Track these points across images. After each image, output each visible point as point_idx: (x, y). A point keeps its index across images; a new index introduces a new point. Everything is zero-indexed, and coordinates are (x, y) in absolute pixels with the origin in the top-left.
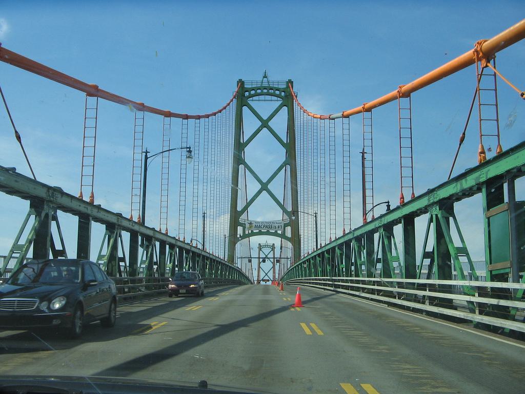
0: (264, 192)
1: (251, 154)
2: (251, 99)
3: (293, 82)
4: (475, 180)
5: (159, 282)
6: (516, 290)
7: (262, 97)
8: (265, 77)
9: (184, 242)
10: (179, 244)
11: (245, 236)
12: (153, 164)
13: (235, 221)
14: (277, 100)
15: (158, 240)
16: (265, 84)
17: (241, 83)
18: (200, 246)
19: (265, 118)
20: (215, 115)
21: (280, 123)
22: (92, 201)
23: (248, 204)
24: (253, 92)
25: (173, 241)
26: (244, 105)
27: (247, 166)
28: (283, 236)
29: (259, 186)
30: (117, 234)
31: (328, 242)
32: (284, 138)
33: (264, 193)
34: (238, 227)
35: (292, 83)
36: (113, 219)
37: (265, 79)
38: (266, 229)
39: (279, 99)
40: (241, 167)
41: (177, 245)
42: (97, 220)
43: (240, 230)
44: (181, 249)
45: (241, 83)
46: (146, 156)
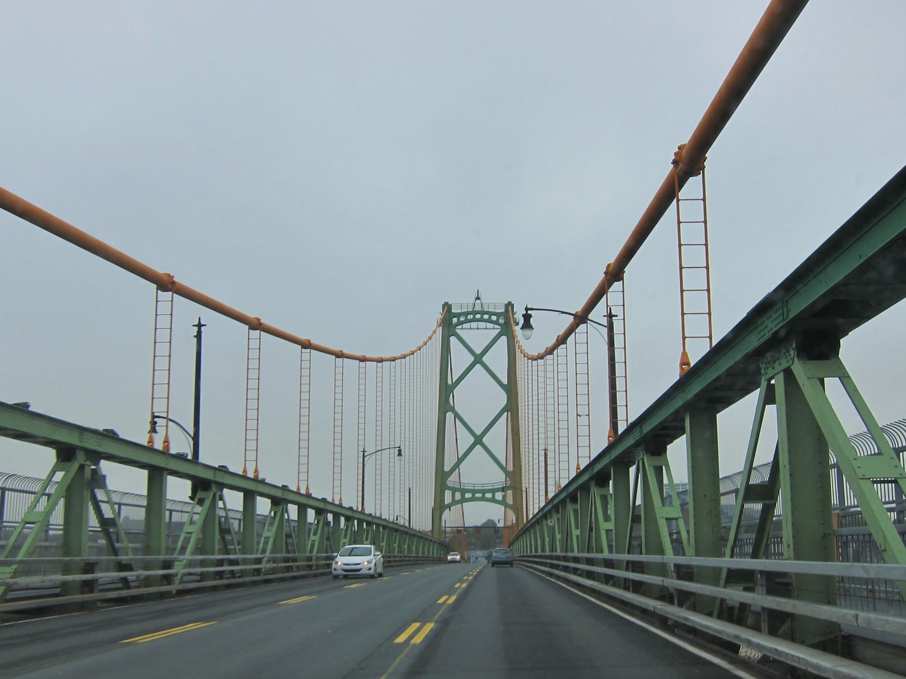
0: (478, 366)
1: (460, 398)
2: (460, 327)
3: (513, 305)
4: (805, 361)
5: (295, 553)
6: (618, 561)
7: (474, 325)
8: (478, 298)
9: (380, 518)
10: (376, 521)
11: (454, 502)
12: (369, 462)
13: (442, 477)
14: (494, 328)
15: (356, 519)
16: (478, 308)
17: (447, 307)
18: (407, 524)
19: (478, 352)
20: (413, 354)
21: (498, 359)
22: (257, 476)
23: (460, 460)
24: (462, 319)
25: (370, 519)
26: (451, 336)
27: (457, 416)
28: (503, 502)
29: (472, 359)
30: (283, 508)
31: (573, 474)
32: (505, 381)
33: (478, 351)
34: (446, 491)
35: (513, 306)
36: (279, 494)
37: (478, 301)
38: (480, 494)
39: (496, 326)
40: (450, 416)
41: (373, 523)
42: (262, 495)
43: (448, 495)
44: (378, 525)
45: (447, 307)
46: (364, 454)
